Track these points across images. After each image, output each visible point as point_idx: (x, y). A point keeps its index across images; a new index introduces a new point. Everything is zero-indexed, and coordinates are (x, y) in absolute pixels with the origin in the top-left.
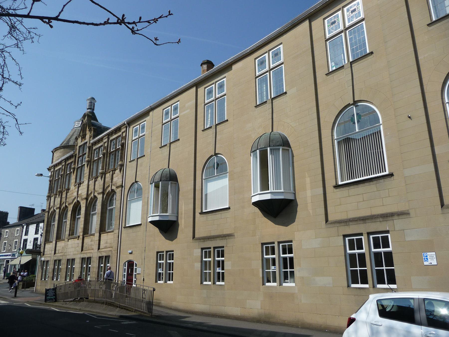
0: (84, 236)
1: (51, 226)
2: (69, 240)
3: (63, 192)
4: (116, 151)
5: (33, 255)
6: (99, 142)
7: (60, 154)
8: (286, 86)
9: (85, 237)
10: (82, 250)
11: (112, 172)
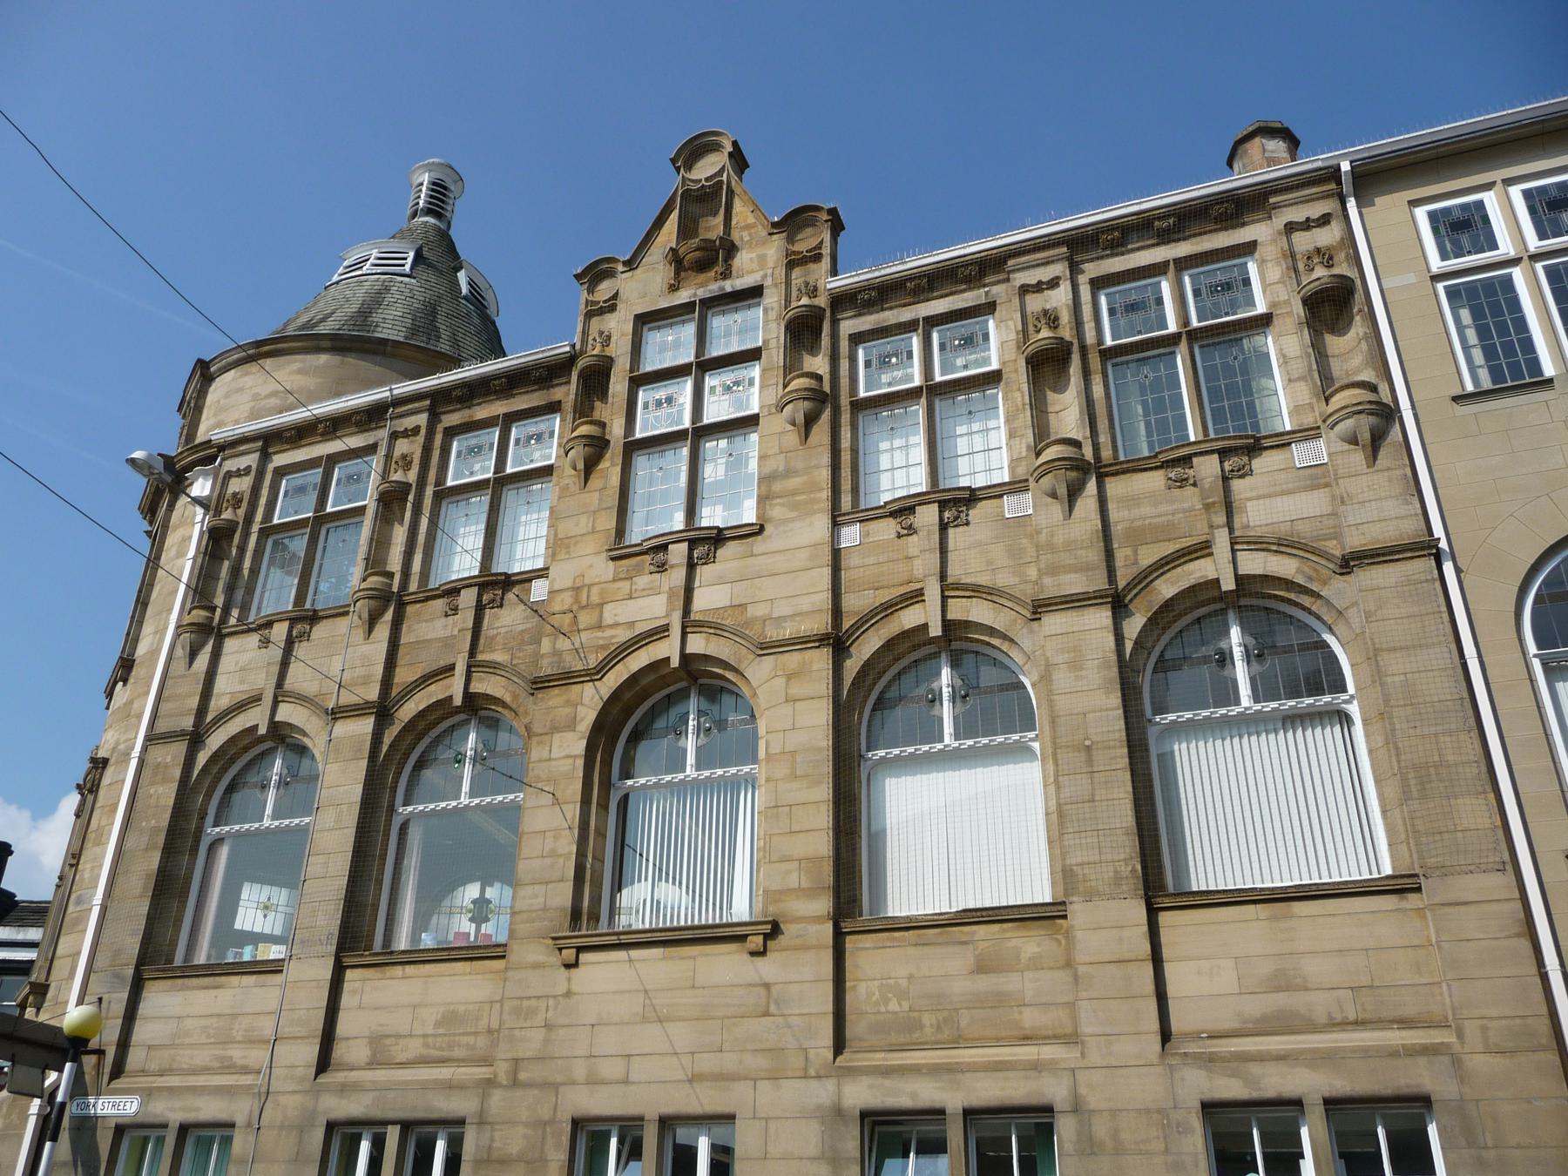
0: (847, 926)
1: (197, 850)
2: (584, 957)
3: (225, 631)
4: (321, 520)
5: (18, 1067)
6: (931, 288)
7: (310, 382)
8: (767, 498)
9: (151, 982)
10: (839, 1046)
11: (286, 624)
